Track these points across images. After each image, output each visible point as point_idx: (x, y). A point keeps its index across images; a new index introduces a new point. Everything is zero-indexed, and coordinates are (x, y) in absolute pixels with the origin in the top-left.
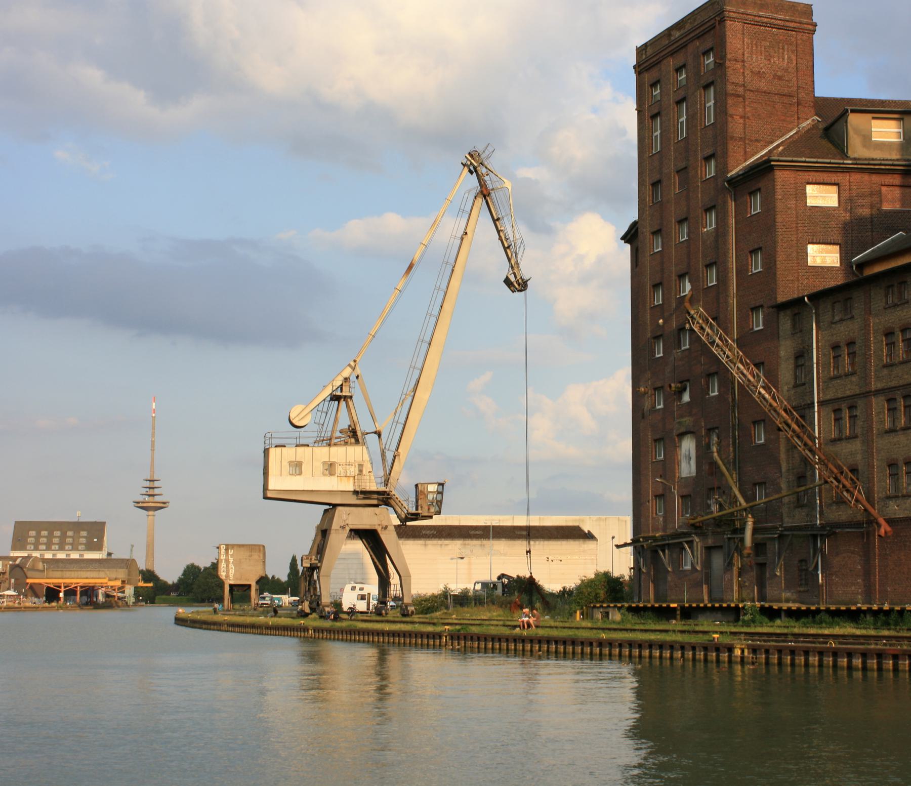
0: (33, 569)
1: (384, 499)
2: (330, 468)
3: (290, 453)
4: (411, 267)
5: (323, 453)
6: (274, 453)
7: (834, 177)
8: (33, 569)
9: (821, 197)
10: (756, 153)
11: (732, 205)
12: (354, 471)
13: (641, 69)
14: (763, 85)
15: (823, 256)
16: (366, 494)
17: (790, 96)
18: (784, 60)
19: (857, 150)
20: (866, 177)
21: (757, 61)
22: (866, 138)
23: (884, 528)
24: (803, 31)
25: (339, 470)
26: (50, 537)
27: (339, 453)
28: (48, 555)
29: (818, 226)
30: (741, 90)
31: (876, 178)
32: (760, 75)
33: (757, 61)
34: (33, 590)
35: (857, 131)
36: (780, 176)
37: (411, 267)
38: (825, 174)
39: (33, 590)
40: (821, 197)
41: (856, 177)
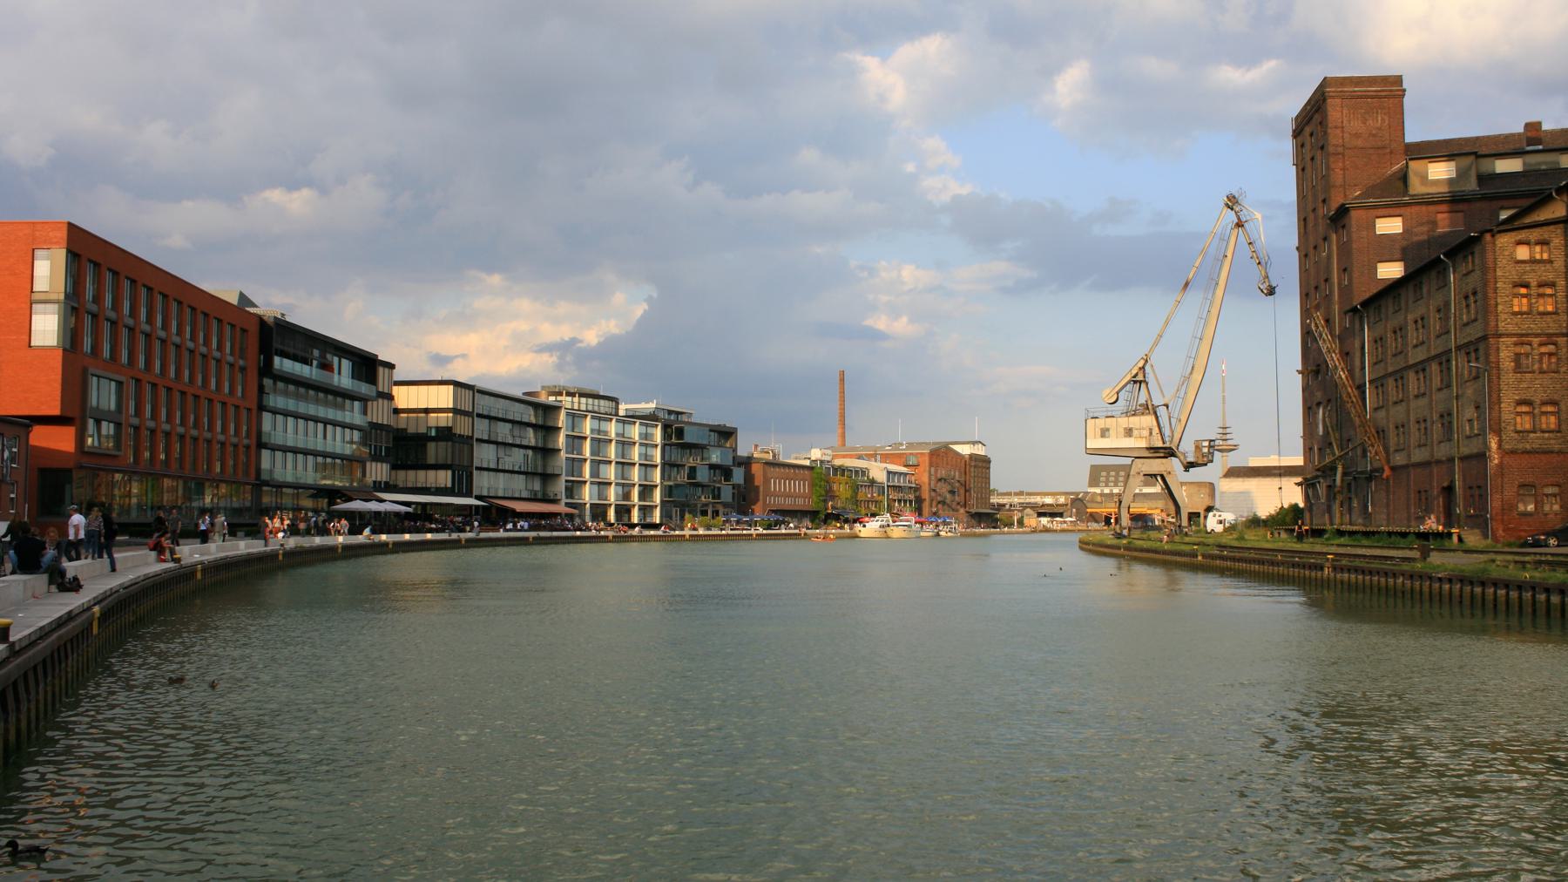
0: (1092, 501)
1: (1170, 453)
2: (1129, 432)
3: (1101, 423)
4: (1187, 284)
5: (1124, 422)
6: (1090, 422)
7: (1398, 211)
8: (1092, 501)
9: (1390, 226)
10: (432, 504)
11: (1334, 237)
12: (1145, 433)
13: (1297, 134)
14: (1359, 143)
15: (1391, 271)
16: (1156, 449)
17: (1384, 148)
18: (1379, 121)
19: (1416, 187)
20: (1424, 208)
21: (1356, 125)
22: (1424, 178)
23: (1387, 472)
24: (1394, 97)
25: (1135, 433)
26: (1117, 476)
27: (1135, 421)
28: (1107, 491)
29: (1387, 248)
30: (1340, 150)
31: (1432, 208)
32: (1357, 135)
33: (1356, 125)
34: (1094, 517)
35: (1416, 174)
36: (1353, 213)
37: (1187, 284)
38: (1390, 210)
39: (1094, 517)
40: (1390, 226)
41: (1415, 209)
